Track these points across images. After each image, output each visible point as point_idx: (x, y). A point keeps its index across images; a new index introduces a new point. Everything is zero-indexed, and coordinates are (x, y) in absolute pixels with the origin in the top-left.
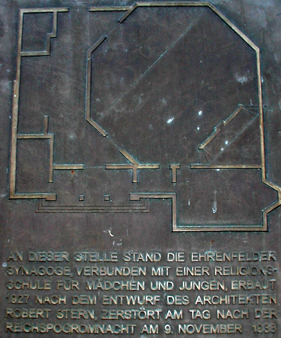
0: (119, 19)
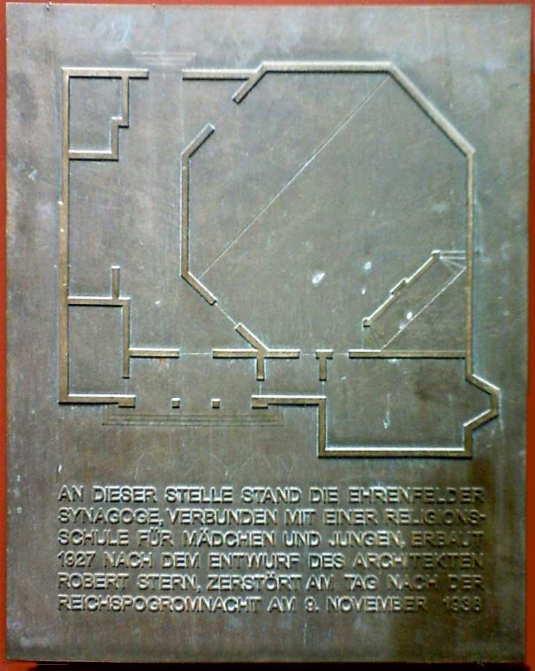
0: (236, 94)
